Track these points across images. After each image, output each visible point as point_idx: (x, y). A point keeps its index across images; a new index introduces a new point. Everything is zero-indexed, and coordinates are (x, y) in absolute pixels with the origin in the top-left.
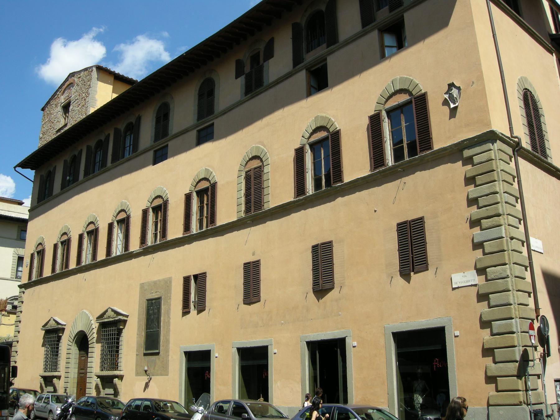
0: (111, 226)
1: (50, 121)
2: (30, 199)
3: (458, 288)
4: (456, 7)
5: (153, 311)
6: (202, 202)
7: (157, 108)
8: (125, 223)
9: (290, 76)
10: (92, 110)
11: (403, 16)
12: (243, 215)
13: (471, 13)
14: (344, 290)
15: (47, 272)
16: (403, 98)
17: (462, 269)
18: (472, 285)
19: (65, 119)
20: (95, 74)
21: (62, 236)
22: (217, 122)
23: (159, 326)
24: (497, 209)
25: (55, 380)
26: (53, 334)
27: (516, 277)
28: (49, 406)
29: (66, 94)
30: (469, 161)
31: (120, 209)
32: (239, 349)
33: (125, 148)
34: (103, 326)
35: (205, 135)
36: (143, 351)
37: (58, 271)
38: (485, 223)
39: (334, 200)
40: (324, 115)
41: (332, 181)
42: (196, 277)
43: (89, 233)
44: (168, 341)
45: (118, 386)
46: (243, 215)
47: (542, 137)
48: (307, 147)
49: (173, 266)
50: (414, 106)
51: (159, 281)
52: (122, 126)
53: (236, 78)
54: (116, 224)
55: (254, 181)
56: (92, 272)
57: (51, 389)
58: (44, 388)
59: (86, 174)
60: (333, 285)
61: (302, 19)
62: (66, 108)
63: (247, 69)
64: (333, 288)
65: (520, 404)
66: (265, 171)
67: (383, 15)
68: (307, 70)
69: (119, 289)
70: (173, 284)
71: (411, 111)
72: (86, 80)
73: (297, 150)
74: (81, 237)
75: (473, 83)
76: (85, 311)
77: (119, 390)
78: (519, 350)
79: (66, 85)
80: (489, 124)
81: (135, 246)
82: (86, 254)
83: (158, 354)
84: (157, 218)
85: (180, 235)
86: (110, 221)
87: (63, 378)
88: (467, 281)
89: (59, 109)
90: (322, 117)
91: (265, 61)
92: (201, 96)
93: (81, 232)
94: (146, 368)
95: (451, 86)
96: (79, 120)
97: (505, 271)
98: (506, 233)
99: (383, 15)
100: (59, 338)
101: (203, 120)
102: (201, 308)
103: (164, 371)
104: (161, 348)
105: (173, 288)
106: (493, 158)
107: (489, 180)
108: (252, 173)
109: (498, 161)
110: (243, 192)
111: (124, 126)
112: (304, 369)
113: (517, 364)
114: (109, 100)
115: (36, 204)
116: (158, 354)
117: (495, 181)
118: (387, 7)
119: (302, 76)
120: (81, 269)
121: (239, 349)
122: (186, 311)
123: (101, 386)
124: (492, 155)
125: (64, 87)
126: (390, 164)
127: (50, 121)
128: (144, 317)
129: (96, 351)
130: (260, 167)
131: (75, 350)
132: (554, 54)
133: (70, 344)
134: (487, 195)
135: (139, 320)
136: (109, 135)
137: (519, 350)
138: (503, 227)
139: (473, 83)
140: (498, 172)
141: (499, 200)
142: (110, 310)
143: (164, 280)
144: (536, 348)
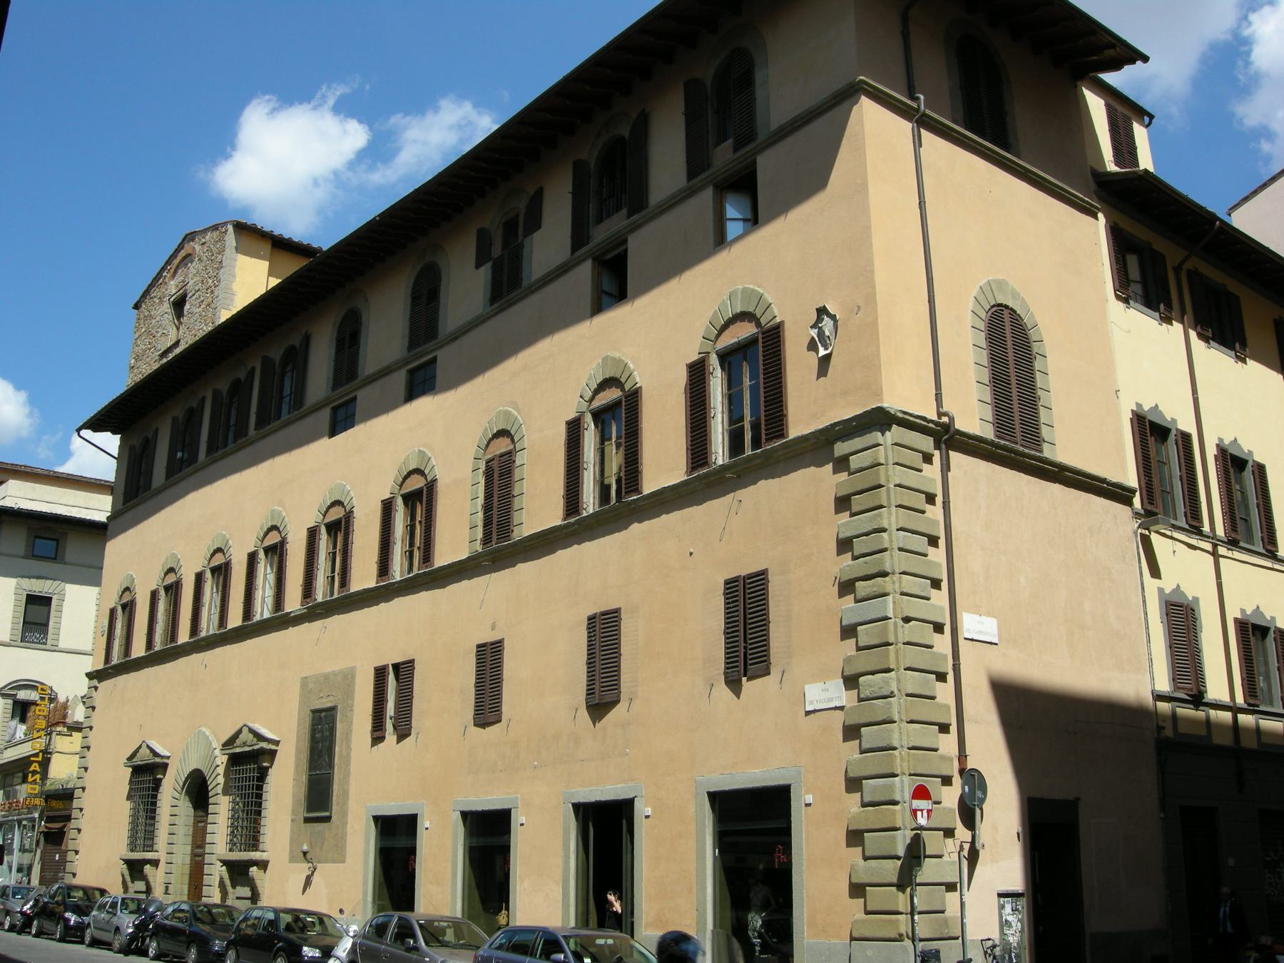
0: (252, 558)
1: (148, 332)
3: (815, 711)
4: (841, 149)
5: (322, 731)
6: (604, 438)
7: (339, 320)
8: (277, 552)
9: (566, 271)
10: (224, 316)
11: (754, 162)
12: (478, 547)
13: (864, 165)
14: (636, 706)
15: (138, 650)
16: (744, 331)
17: (821, 676)
18: (836, 708)
19: (178, 329)
20: (231, 238)
21: (166, 574)
22: (441, 355)
23: (331, 765)
24: (881, 562)
25: (147, 868)
26: (146, 773)
27: (908, 695)
28: (115, 920)
29: (179, 278)
30: (842, 464)
31: (270, 524)
32: (465, 815)
33: (282, 398)
34: (235, 760)
35: (421, 382)
36: (302, 813)
37: (158, 646)
38: (863, 588)
39: (626, 528)
40: (617, 355)
41: (763, 437)
42: (396, 667)
43: (216, 571)
44: (345, 794)
45: (258, 882)
46: (478, 547)
47: (1030, 401)
48: (588, 419)
49: (352, 647)
50: (761, 349)
51: (334, 673)
52: (276, 354)
53: (478, 266)
54: (261, 555)
55: (499, 478)
56: (218, 651)
57: (141, 886)
58: (130, 884)
59: (212, 449)
60: (619, 696)
61: (590, 153)
62: (179, 305)
63: (497, 251)
64: (618, 701)
65: (899, 938)
66: (518, 463)
67: (723, 156)
68: (594, 259)
69: (259, 689)
70: (358, 681)
71: (754, 355)
72: (214, 249)
73: (569, 423)
74: (199, 578)
75: (859, 308)
76: (204, 729)
77: (260, 890)
78: (904, 836)
79: (179, 259)
80: (878, 394)
81: (293, 603)
82: (210, 614)
83: (328, 819)
84: (413, 518)
85: (371, 583)
86: (252, 549)
87: (162, 865)
88: (830, 700)
89: (167, 307)
90: (613, 359)
91: (525, 236)
92: (415, 298)
93: (199, 570)
94: (305, 848)
95: (822, 311)
96: (200, 334)
97: (887, 682)
98: (894, 609)
99: (723, 156)
100: (157, 784)
101: (420, 349)
102: (403, 733)
103: (339, 855)
104: (334, 808)
105: (357, 687)
106: (882, 461)
107: (872, 505)
108: (495, 464)
109: (891, 466)
110: (481, 501)
111: (282, 351)
112: (567, 857)
113: (899, 863)
114: (260, 291)
115: (120, 506)
116: (328, 819)
117: (881, 507)
118: (730, 141)
119: (585, 271)
120: (200, 645)
121: (465, 815)
122: (378, 739)
123: (228, 882)
124: (880, 454)
125: (176, 261)
126: (720, 462)
127: (148, 332)
128: (306, 745)
129: (222, 808)
130: (509, 453)
131: (186, 808)
132: (1100, 215)
133: (177, 795)
134: (867, 534)
136: (253, 369)
137: (904, 836)
138: (890, 598)
139: (859, 308)
140: (888, 489)
141: (886, 545)
142: (245, 730)
143: (341, 671)
144: (949, 833)
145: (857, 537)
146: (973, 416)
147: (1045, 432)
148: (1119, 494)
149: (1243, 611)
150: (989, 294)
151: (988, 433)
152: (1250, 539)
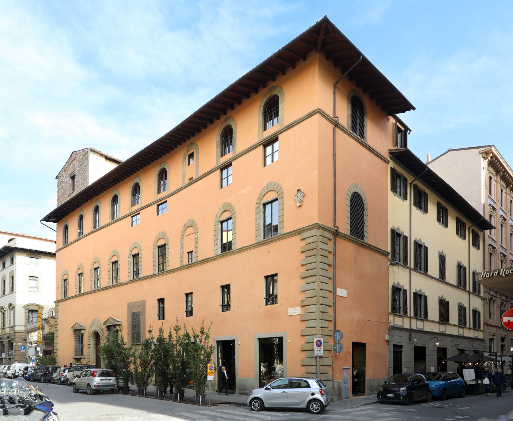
2: (366, 378)
26: (78, 333)
135: (366, 133)
142: (110, 319)
145: (154, 275)
146: (345, 228)
147: (365, 234)
148: (385, 254)
149: (416, 290)
150: (352, 188)
151: (348, 233)
152: (421, 270)
